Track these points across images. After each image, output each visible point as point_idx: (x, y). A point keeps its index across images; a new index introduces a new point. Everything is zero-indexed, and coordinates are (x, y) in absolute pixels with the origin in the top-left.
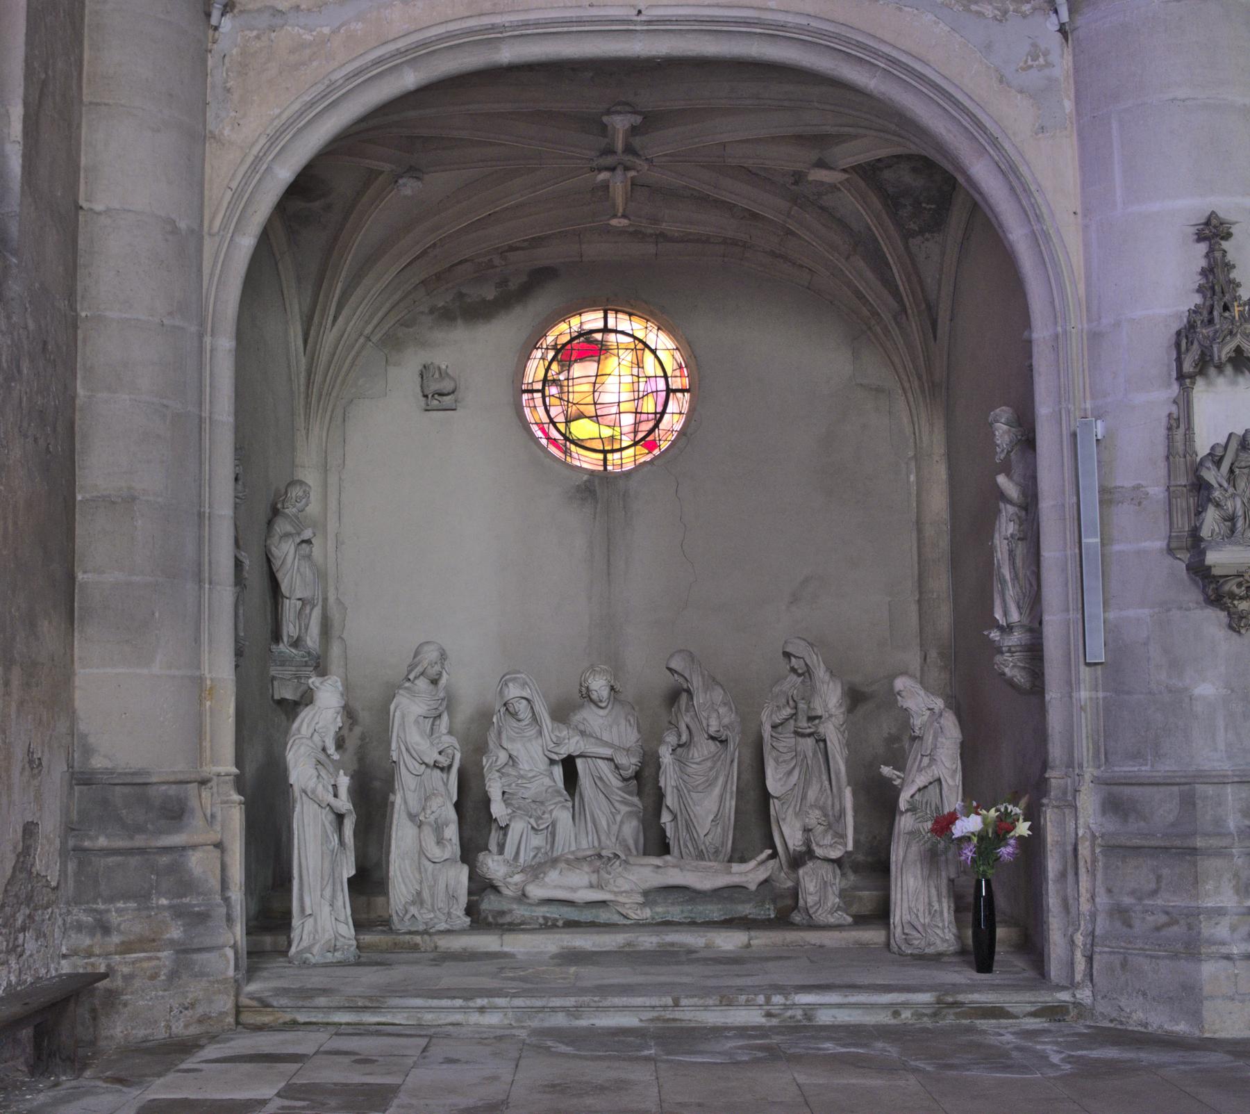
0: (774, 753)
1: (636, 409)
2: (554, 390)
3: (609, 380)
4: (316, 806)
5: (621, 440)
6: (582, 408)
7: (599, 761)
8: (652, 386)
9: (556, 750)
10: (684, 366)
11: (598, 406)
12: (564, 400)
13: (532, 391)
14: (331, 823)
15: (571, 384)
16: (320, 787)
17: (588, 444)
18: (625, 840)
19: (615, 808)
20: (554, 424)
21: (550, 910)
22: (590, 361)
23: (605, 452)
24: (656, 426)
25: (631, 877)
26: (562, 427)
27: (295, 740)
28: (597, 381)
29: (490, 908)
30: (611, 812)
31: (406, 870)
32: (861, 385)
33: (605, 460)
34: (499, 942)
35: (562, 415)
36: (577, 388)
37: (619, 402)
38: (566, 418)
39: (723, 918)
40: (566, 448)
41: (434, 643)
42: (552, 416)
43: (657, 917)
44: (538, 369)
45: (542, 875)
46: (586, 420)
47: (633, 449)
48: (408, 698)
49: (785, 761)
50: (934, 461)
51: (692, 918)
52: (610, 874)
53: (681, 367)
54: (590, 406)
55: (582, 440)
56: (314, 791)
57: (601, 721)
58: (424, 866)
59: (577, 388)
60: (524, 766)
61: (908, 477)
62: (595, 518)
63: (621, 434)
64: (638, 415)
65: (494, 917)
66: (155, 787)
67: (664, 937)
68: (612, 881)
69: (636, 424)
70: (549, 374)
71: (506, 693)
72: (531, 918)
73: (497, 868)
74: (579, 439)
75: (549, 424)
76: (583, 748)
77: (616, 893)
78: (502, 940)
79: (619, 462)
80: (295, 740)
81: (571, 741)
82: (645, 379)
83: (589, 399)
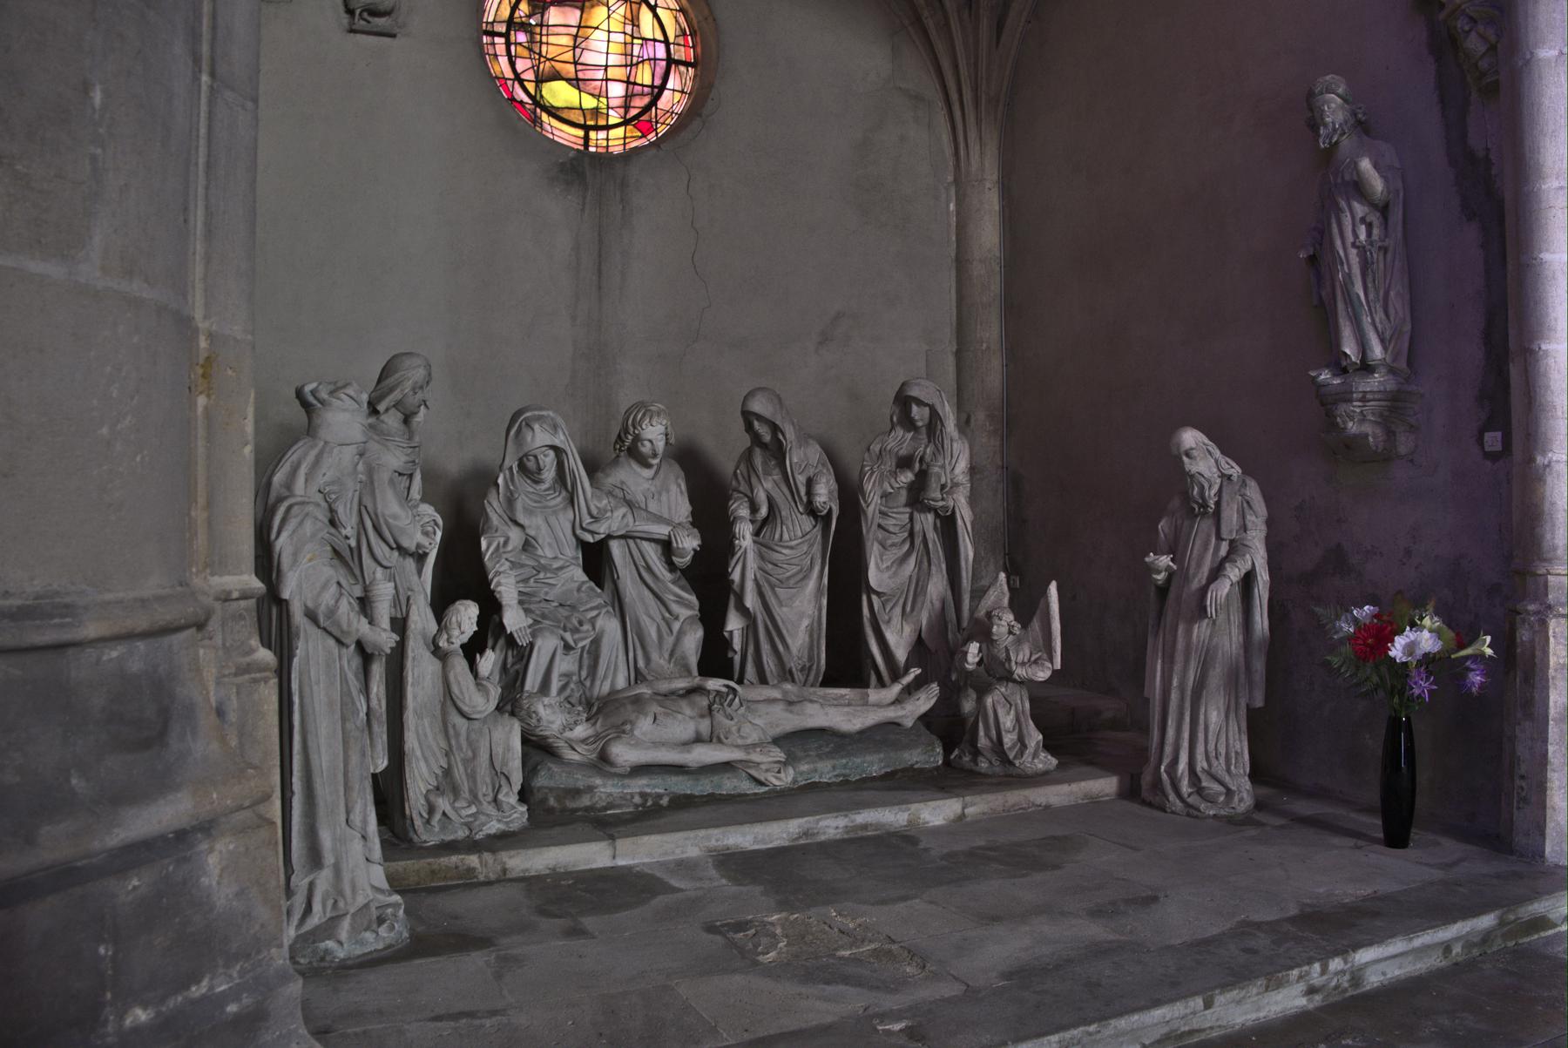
0: (881, 534)
1: (628, 78)
2: (522, 37)
3: (597, 35)
4: (331, 642)
5: (608, 115)
6: (558, 66)
7: (646, 545)
8: (649, 52)
9: (593, 527)
10: (688, 33)
11: (579, 67)
12: (535, 53)
13: (493, 34)
14: (356, 676)
15: (544, 32)
16: (344, 606)
17: (565, 115)
18: (684, 658)
19: (670, 613)
20: (521, 82)
21: (653, 782)
22: (570, 6)
23: (587, 128)
24: (654, 102)
25: (757, 721)
26: (531, 87)
27: (289, 509)
28: (580, 34)
29: (552, 784)
30: (664, 618)
31: (425, 735)
32: (900, 88)
33: (586, 138)
34: (609, 852)
35: (531, 71)
36: (552, 39)
37: (607, 67)
38: (537, 76)
39: (883, 772)
40: (536, 116)
41: (418, 355)
42: (519, 71)
43: (799, 779)
44: (502, 6)
45: (628, 727)
46: (563, 83)
47: (622, 129)
48: (378, 442)
49: (893, 545)
50: (986, 190)
51: (844, 775)
52: (732, 719)
53: (684, 34)
54: (568, 65)
55: (558, 108)
56: (331, 613)
57: (646, 486)
58: (454, 726)
59: (552, 39)
60: (546, 552)
61: (948, 206)
62: (583, 210)
63: (608, 108)
64: (631, 87)
65: (558, 799)
66: (91, 653)
67: (853, 817)
68: (734, 729)
69: (628, 97)
70: (517, 15)
71: (529, 438)
72: (623, 798)
73: (552, 718)
74: (553, 107)
75: (514, 80)
76: (631, 524)
77: (748, 748)
78: (615, 848)
79: (605, 143)
80: (289, 509)
81: (616, 514)
82: (640, 41)
83: (568, 56)
